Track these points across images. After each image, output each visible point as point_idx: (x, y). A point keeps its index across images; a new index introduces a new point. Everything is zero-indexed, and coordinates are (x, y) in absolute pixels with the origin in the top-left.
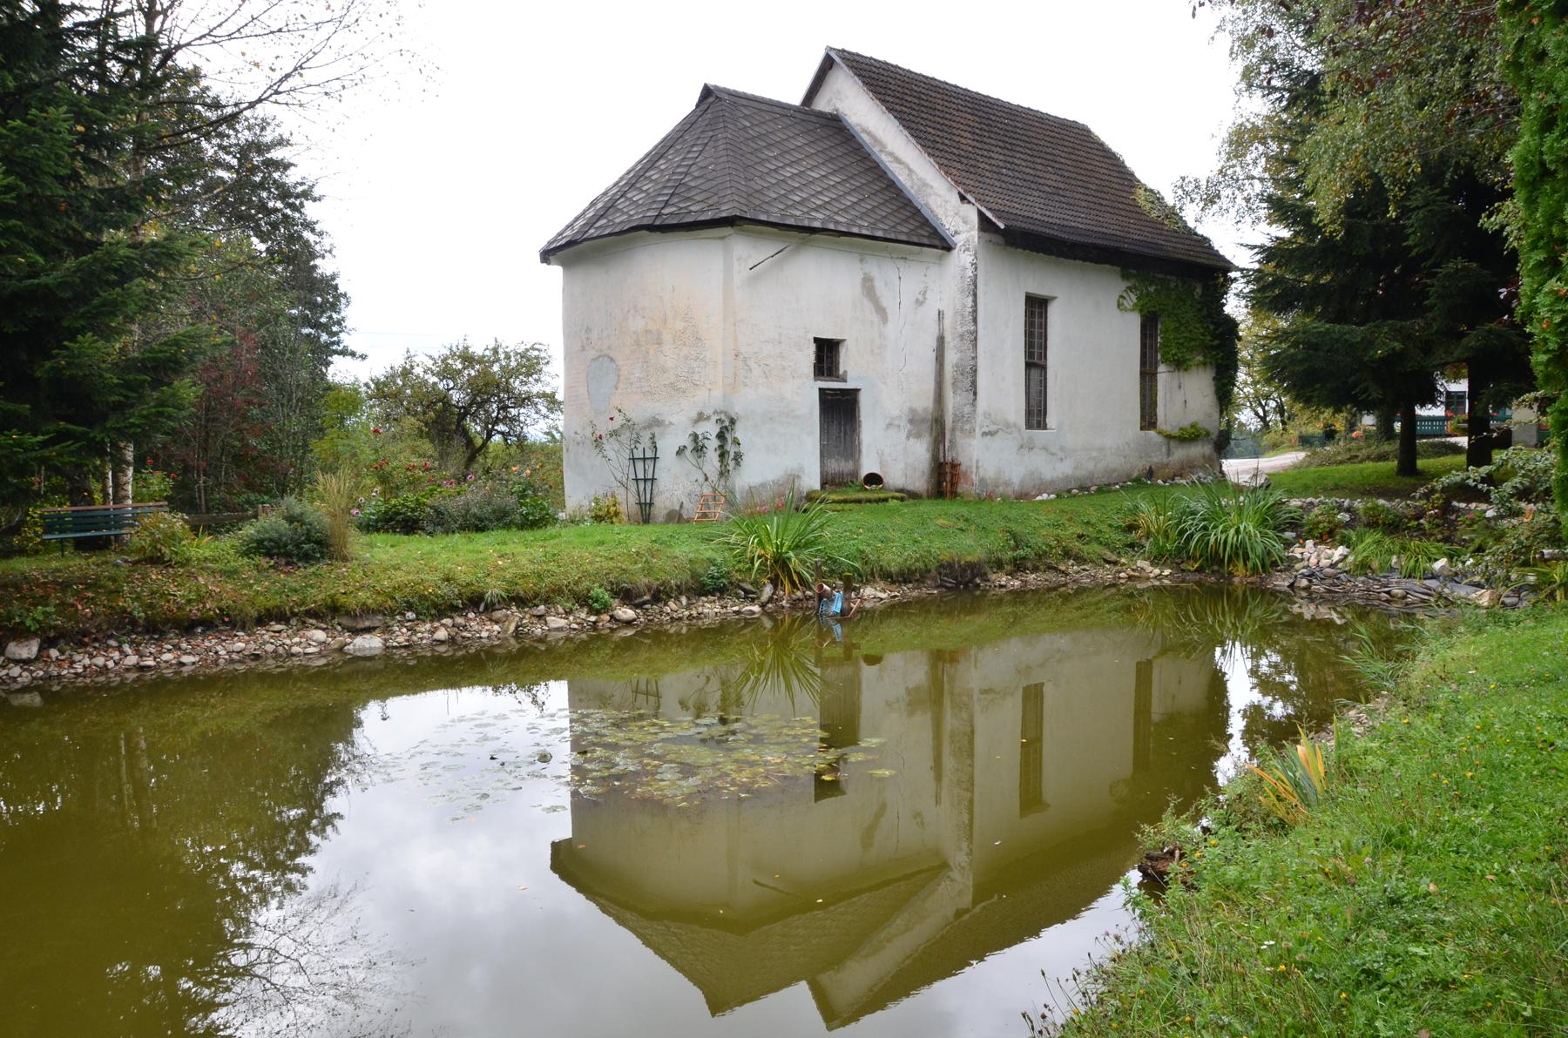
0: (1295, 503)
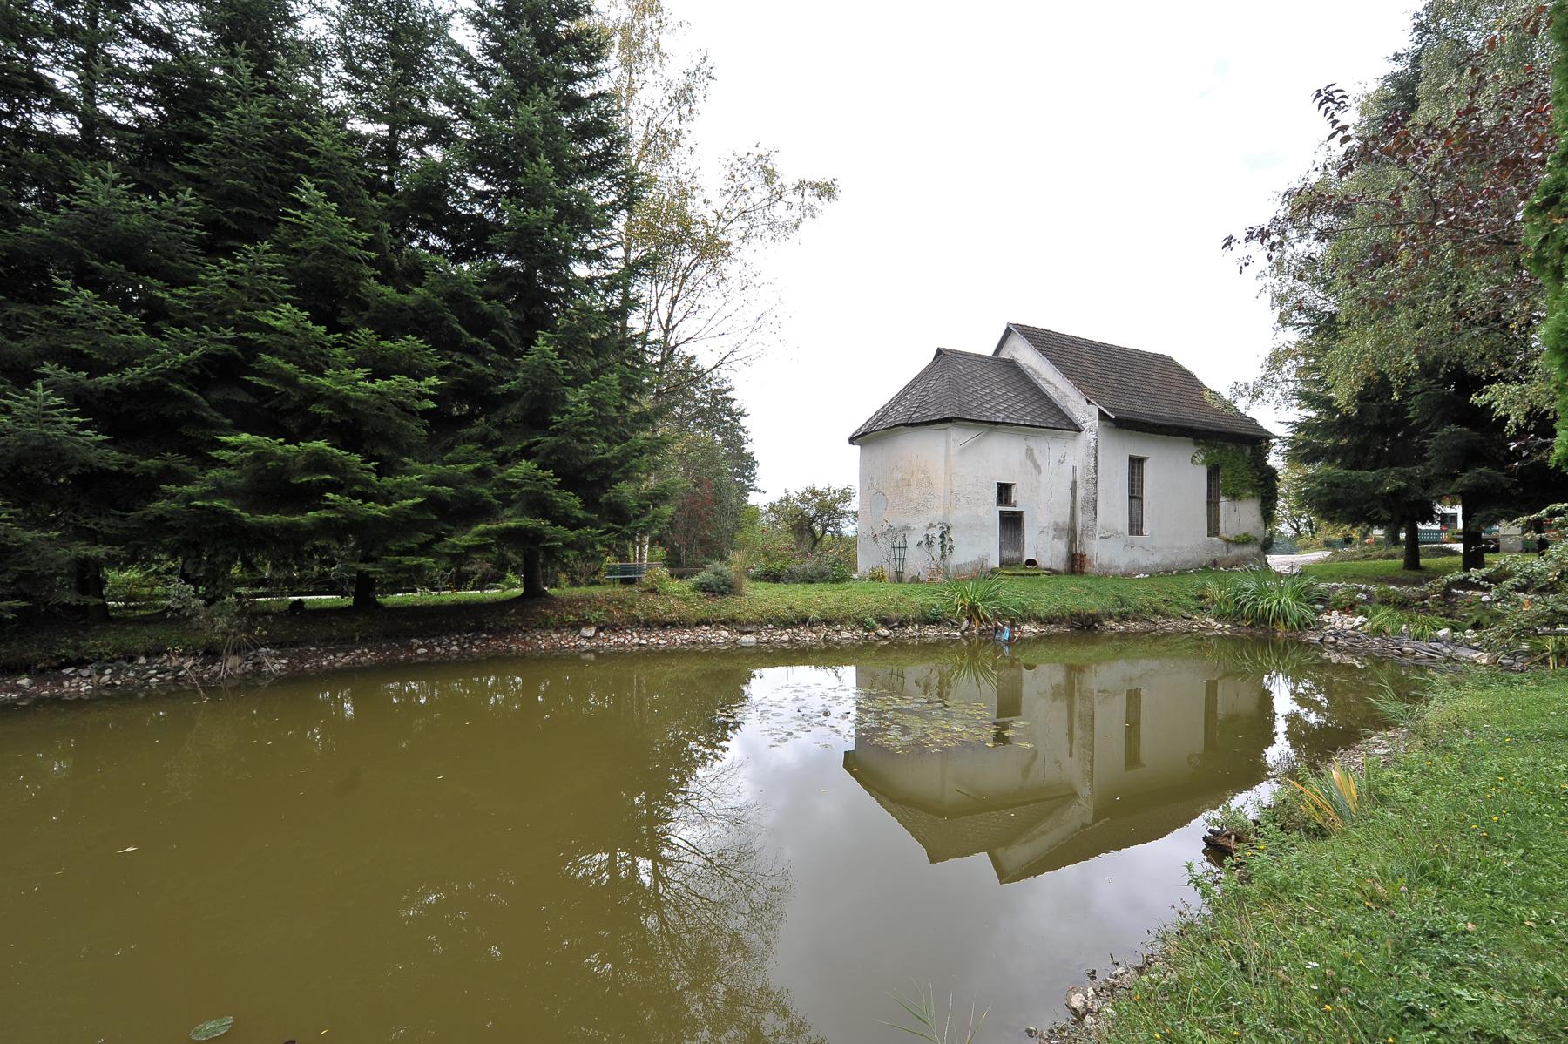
0: (1322, 586)
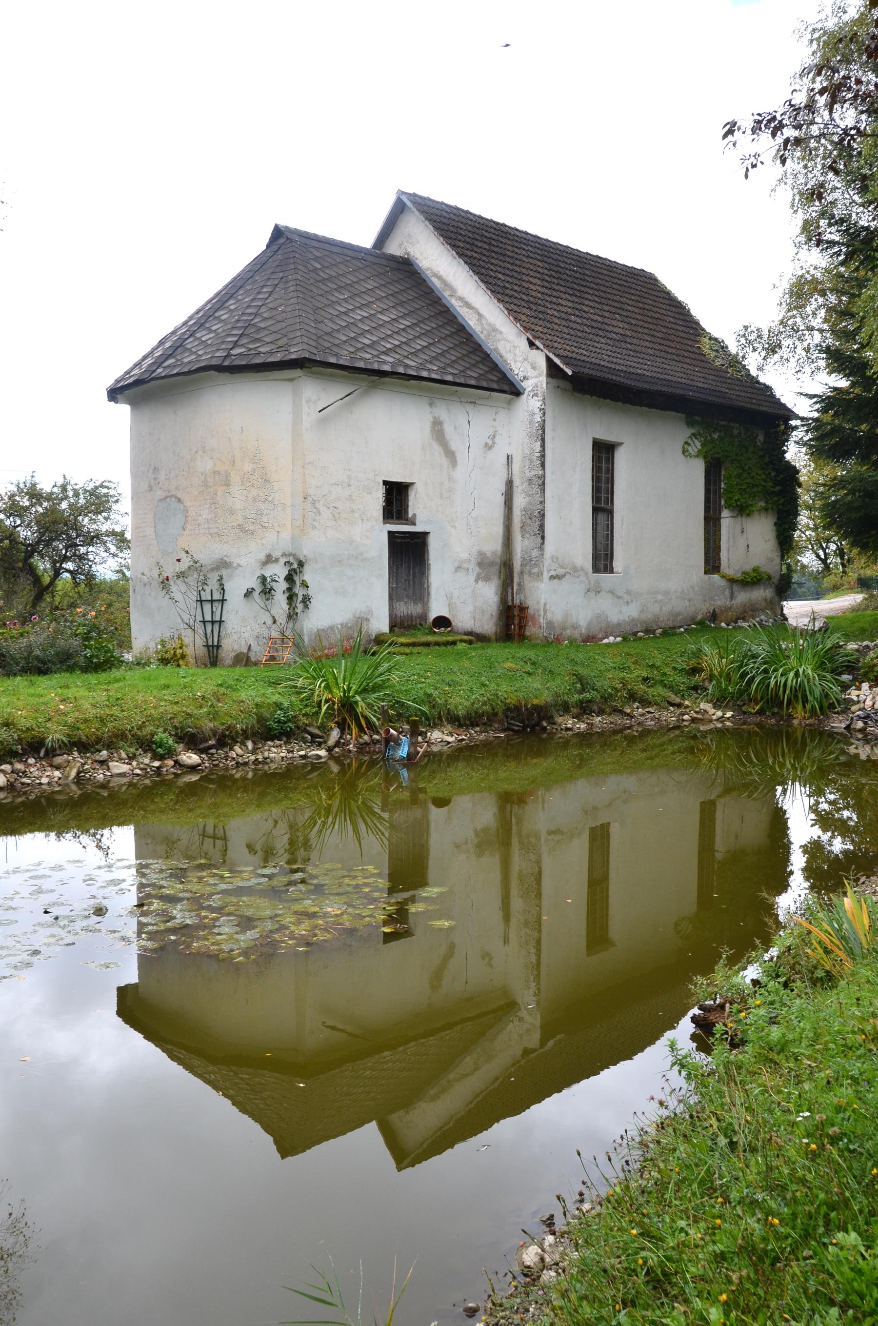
0: (852, 646)
